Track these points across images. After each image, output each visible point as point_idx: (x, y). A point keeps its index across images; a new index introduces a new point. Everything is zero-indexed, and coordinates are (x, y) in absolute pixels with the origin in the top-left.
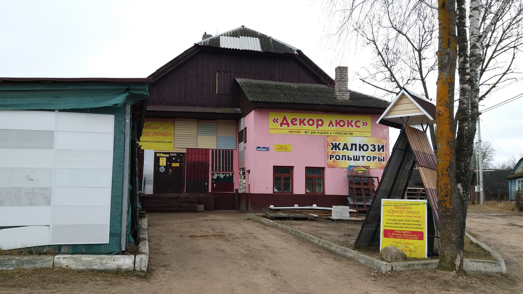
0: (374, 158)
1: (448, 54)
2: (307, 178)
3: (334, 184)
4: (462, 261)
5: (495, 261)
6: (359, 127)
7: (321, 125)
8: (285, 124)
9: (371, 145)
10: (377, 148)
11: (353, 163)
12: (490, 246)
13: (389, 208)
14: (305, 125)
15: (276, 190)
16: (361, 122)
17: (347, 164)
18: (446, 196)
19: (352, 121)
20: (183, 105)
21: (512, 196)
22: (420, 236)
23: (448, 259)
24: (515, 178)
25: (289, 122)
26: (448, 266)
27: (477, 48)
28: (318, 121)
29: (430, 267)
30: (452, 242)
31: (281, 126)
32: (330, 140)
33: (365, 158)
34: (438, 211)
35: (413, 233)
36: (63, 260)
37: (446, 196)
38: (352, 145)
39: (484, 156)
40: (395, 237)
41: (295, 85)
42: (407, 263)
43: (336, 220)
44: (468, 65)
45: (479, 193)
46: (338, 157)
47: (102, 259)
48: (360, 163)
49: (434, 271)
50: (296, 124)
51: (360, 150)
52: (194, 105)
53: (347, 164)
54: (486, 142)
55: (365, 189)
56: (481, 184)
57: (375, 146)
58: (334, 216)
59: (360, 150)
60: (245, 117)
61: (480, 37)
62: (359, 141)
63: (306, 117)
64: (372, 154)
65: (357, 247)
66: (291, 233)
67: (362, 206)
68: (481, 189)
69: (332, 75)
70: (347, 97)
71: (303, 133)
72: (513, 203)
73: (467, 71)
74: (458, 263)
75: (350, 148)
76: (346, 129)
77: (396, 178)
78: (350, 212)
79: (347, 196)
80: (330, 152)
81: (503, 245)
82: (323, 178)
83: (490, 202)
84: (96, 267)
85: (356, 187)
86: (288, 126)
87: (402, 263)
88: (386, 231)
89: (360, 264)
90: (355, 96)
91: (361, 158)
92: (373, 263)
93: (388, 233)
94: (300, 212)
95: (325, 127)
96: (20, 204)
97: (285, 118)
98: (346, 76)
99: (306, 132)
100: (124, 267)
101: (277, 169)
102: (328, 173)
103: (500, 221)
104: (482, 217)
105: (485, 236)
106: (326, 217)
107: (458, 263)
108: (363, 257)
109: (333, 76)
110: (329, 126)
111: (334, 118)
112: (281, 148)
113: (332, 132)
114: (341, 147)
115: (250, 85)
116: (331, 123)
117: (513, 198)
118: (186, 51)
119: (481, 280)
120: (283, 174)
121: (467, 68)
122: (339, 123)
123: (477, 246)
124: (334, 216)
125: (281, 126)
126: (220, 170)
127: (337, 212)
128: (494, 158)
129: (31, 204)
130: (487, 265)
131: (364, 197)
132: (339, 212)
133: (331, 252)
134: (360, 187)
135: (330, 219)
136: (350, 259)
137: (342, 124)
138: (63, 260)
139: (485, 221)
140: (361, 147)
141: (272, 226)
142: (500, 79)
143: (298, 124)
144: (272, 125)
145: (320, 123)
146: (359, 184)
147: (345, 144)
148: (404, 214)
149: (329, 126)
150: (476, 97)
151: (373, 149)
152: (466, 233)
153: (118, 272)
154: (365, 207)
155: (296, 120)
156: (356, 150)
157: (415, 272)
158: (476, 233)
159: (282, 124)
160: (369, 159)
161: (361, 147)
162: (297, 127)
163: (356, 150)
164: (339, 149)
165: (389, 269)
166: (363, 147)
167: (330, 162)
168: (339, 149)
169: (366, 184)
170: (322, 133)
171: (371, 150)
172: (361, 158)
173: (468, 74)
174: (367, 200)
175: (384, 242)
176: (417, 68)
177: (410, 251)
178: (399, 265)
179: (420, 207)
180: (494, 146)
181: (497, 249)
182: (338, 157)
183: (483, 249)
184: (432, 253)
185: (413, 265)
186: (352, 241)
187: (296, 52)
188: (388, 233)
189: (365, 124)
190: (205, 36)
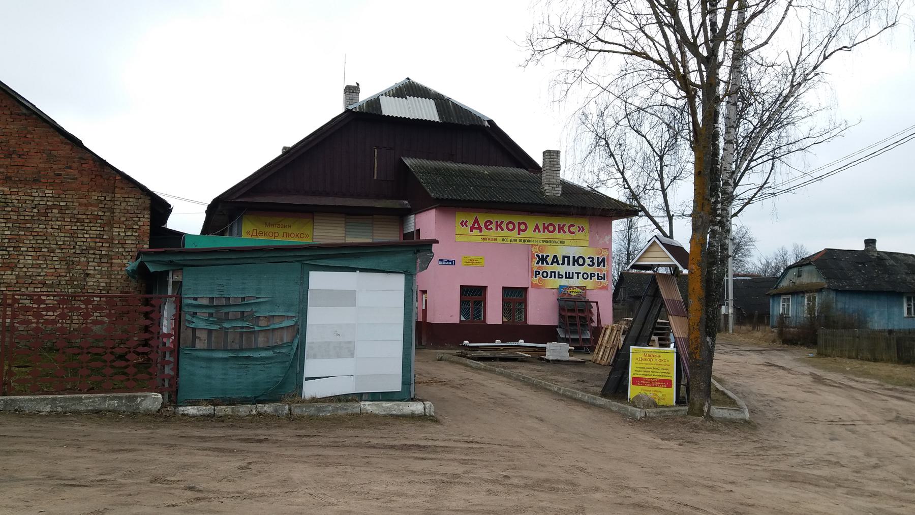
0: (592, 275)
1: (701, 217)
2: (505, 302)
3: (540, 311)
4: (709, 408)
5: (740, 409)
6: (573, 233)
8: (476, 228)
10: (595, 261)
11: (564, 282)
12: (737, 393)
13: (638, 356)
14: (502, 229)
15: (463, 319)
17: (556, 283)
18: (696, 348)
19: (564, 225)
20: (327, 194)
21: (774, 320)
22: (668, 384)
23: (697, 406)
24: (779, 295)
25: (482, 225)
26: (697, 412)
27: (730, 185)
28: (519, 224)
29: (679, 413)
30: (701, 391)
31: (471, 231)
32: (535, 250)
33: (580, 276)
34: (688, 361)
35: (662, 381)
36: (368, 406)
37: (696, 348)
38: (564, 257)
39: (738, 248)
40: (643, 385)
41: (485, 170)
42: (659, 410)
43: (553, 360)
44: (719, 206)
45: (726, 316)
46: (545, 275)
47: (399, 405)
48: (575, 282)
49: (684, 416)
50: (491, 229)
51: (574, 265)
52: (344, 195)
53: (556, 283)
54: (742, 227)
55: (581, 318)
56: (731, 303)
57: (593, 259)
58: (549, 356)
59: (574, 265)
60: (418, 215)
61: (733, 172)
62: (573, 252)
63: (505, 219)
64: (590, 270)
65: (604, 394)
66: (517, 379)
67: (577, 340)
68: (731, 311)
69: (539, 160)
70: (558, 191)
71: (499, 240)
72: (775, 330)
73: (719, 212)
74: (706, 409)
75: (561, 262)
76: (557, 235)
77: (643, 324)
78: (570, 351)
79: (556, 327)
80: (535, 267)
81: (751, 393)
82: (525, 301)
83: (744, 328)
84: (394, 413)
85: (569, 314)
86: (481, 231)
87: (655, 410)
88: (634, 379)
89: (612, 411)
90: (570, 189)
91: (575, 276)
92: (626, 410)
93: (636, 381)
94: (504, 350)
95: (529, 234)
96: (329, 357)
97: (476, 221)
98: (558, 163)
99: (504, 240)
100: (417, 413)
101: (465, 290)
102: (532, 295)
103: (756, 358)
104: (731, 353)
105: (732, 381)
106: (539, 357)
107: (706, 409)
108: (615, 405)
109: (540, 162)
110: (534, 231)
111: (541, 221)
112: (472, 262)
114: (550, 260)
115: (425, 171)
116: (537, 227)
117: (775, 324)
118: (333, 120)
119: (726, 425)
120: (473, 296)
121: (718, 209)
122: (547, 228)
123: (723, 393)
124: (549, 356)
125: (471, 231)
127: (554, 351)
128: (753, 252)
129: (339, 357)
130: (731, 412)
131: (579, 328)
132: (556, 350)
133: (576, 400)
134: (573, 314)
135: (543, 359)
136: (600, 407)
137: (551, 228)
138: (368, 406)
139: (735, 358)
140: (576, 261)
141: (485, 370)
142: (756, 194)
143: (494, 228)
144: (460, 230)
145: (523, 227)
146: (573, 310)
147: (555, 257)
148: (653, 362)
149: (534, 231)
150: (726, 238)
152: (712, 380)
153: (413, 417)
154: (581, 341)
155: (491, 223)
156: (569, 264)
157: (667, 417)
158: (722, 377)
159: (472, 229)
160: (585, 276)
161: (576, 261)
162: (492, 233)
163: (569, 264)
164: (547, 263)
165: (643, 415)
166: (577, 261)
167: (536, 280)
168: (547, 263)
169: (582, 311)
170: (525, 241)
172: (575, 276)
173: (719, 215)
174: (583, 333)
175: (633, 391)
176: (657, 177)
177: (659, 399)
178: (652, 412)
179: (669, 355)
180: (753, 234)
181: (745, 397)
182: (545, 275)
183: (729, 397)
184: (679, 401)
185: (664, 412)
186: (599, 390)
187: (486, 124)
188: (636, 381)
189: (581, 229)
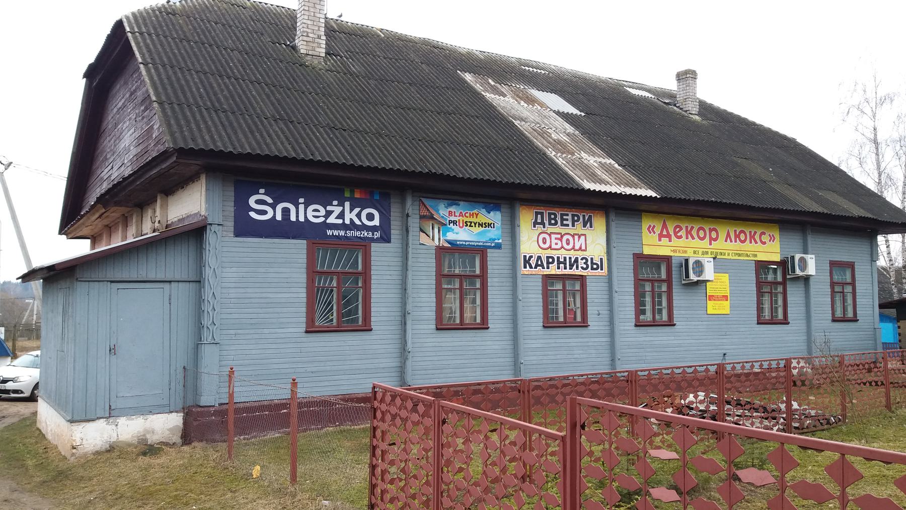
7: (716, 240)
9: (582, 259)
16: (767, 234)
25: (671, 233)
50: (680, 237)
86: (670, 241)
110: (726, 241)
113: (731, 252)
116: (728, 235)
125: (660, 240)
126: (327, 290)
137: (742, 237)
143: (684, 237)
147: (539, 258)
149: (726, 241)
151: (585, 266)
155: (681, 229)
171: (582, 268)
189: (772, 238)
190: (686, 77)
